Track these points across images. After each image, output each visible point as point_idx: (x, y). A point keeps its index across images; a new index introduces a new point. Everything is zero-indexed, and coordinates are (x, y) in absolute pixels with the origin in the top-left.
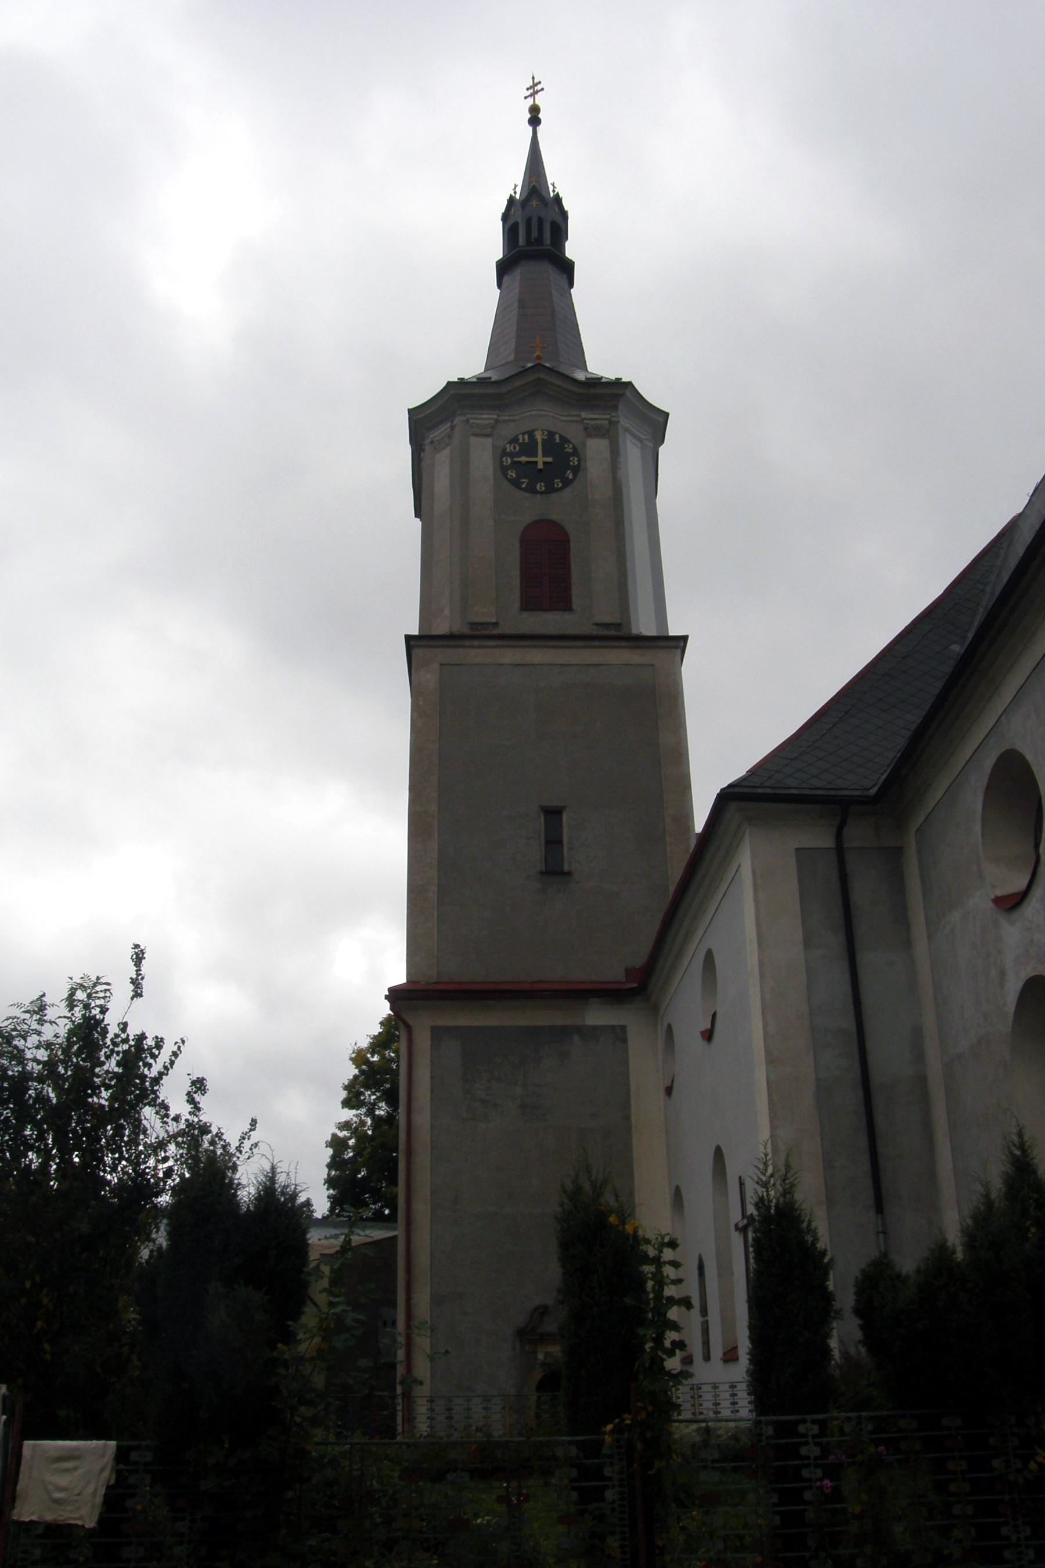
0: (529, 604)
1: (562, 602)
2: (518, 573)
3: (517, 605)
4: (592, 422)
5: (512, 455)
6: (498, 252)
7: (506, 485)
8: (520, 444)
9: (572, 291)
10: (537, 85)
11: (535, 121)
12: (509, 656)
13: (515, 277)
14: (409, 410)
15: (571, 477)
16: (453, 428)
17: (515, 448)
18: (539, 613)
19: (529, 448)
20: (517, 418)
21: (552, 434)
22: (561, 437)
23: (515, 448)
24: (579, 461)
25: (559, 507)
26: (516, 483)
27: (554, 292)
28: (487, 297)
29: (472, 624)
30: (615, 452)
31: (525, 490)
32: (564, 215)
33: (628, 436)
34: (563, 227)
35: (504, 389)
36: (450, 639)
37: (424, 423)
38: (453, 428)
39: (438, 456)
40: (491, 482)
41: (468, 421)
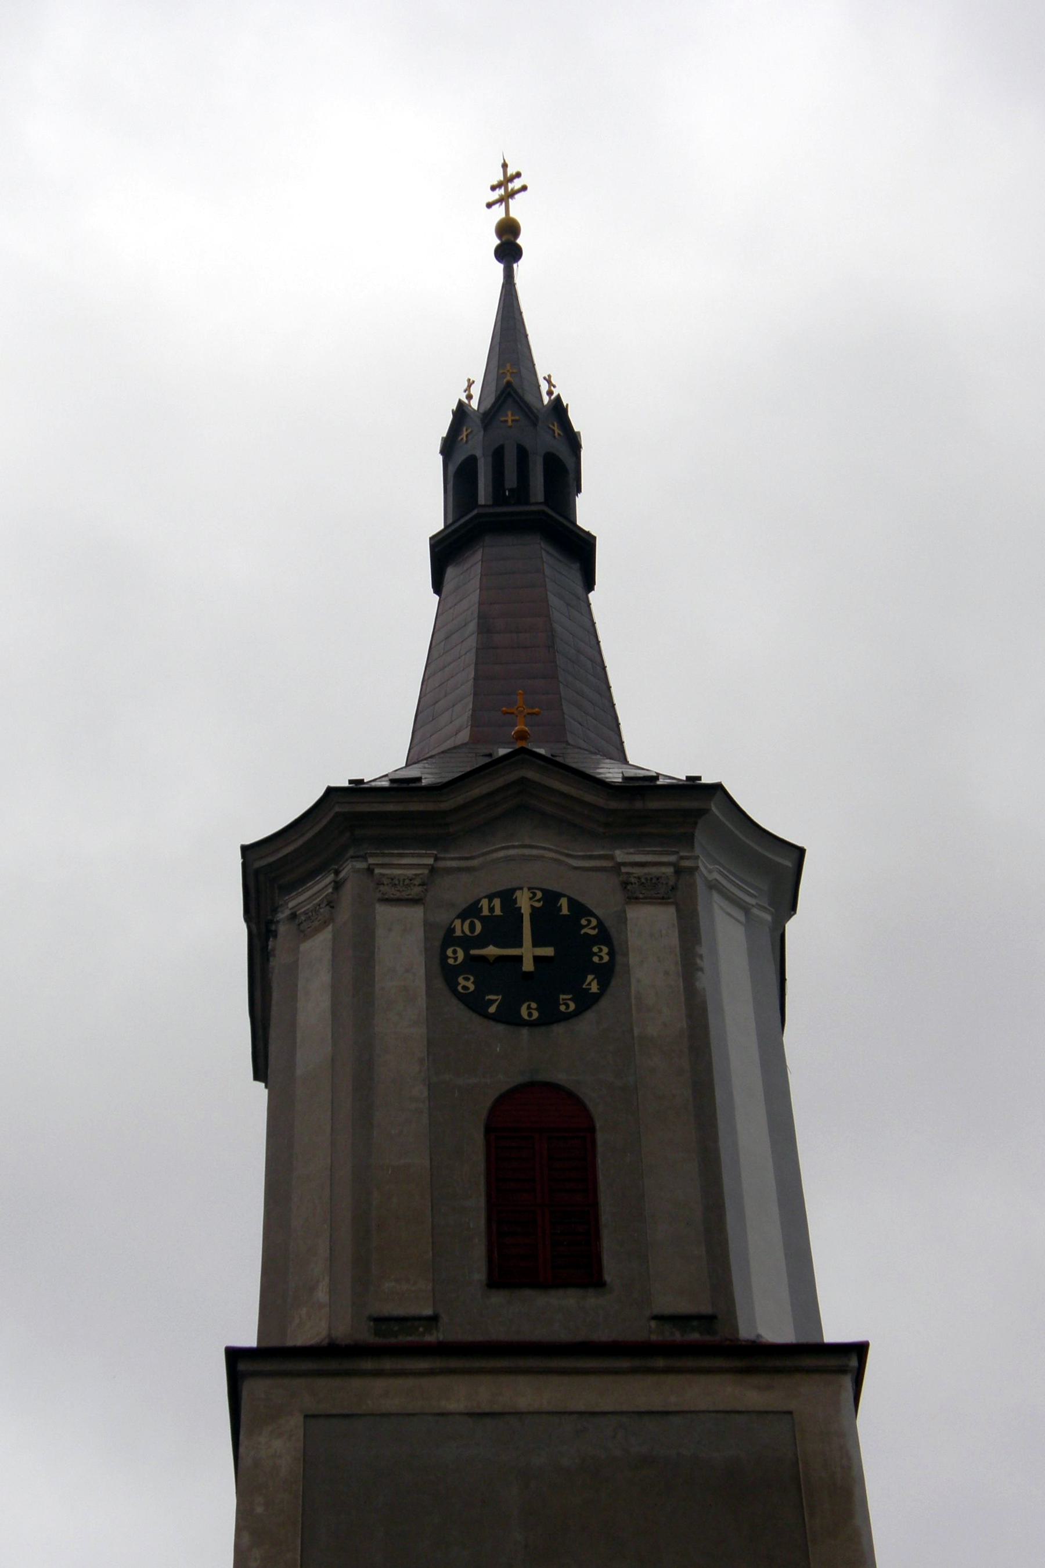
0: (507, 1272)
1: (584, 1271)
2: (482, 1202)
3: (480, 1275)
4: (637, 871)
5: (465, 942)
6: (431, 515)
7: (456, 1009)
8: (483, 919)
9: (591, 596)
10: (511, 179)
11: (508, 250)
12: (462, 1393)
13: (468, 573)
14: (245, 850)
15: (594, 988)
16: (338, 886)
17: (472, 927)
18: (528, 1293)
19: (504, 928)
20: (475, 863)
21: (551, 897)
22: (572, 902)
23: (472, 927)
24: (612, 954)
25: (569, 1054)
26: (474, 1003)
27: (553, 600)
28: (406, 613)
29: (378, 1320)
30: (690, 933)
31: (494, 1018)
32: (573, 442)
33: (716, 897)
34: (569, 463)
35: (447, 804)
36: (331, 1356)
37: (278, 875)
38: (338, 886)
39: (305, 946)
40: (422, 1001)
41: (370, 870)
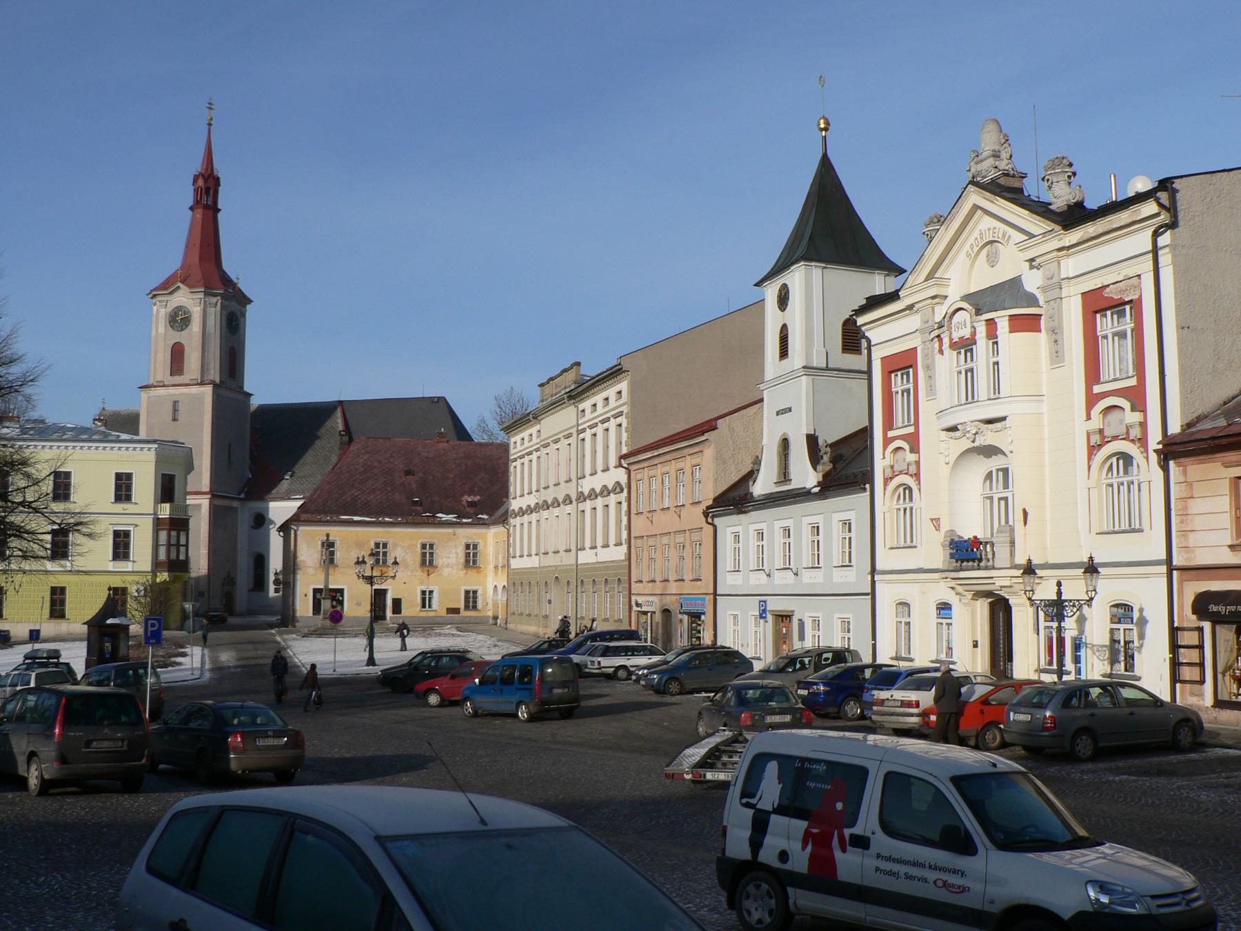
11: (210, 125)
